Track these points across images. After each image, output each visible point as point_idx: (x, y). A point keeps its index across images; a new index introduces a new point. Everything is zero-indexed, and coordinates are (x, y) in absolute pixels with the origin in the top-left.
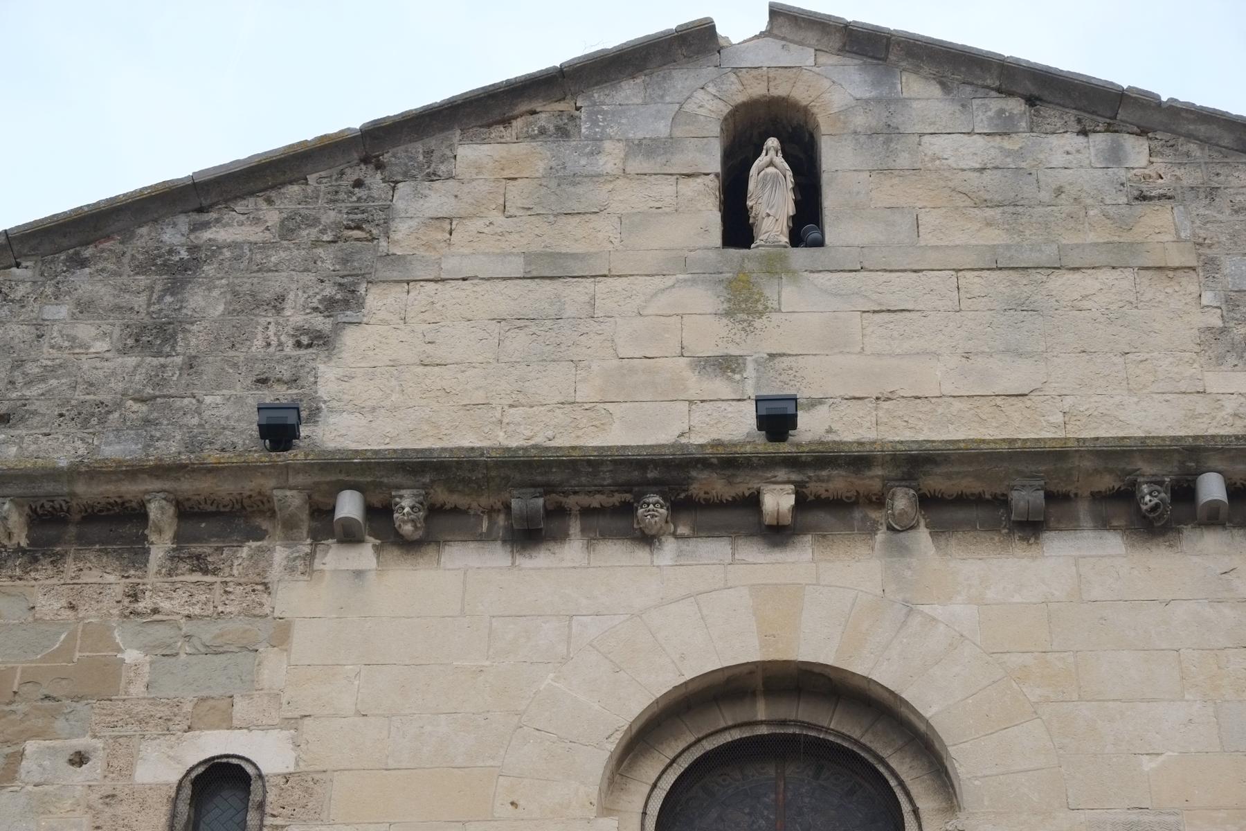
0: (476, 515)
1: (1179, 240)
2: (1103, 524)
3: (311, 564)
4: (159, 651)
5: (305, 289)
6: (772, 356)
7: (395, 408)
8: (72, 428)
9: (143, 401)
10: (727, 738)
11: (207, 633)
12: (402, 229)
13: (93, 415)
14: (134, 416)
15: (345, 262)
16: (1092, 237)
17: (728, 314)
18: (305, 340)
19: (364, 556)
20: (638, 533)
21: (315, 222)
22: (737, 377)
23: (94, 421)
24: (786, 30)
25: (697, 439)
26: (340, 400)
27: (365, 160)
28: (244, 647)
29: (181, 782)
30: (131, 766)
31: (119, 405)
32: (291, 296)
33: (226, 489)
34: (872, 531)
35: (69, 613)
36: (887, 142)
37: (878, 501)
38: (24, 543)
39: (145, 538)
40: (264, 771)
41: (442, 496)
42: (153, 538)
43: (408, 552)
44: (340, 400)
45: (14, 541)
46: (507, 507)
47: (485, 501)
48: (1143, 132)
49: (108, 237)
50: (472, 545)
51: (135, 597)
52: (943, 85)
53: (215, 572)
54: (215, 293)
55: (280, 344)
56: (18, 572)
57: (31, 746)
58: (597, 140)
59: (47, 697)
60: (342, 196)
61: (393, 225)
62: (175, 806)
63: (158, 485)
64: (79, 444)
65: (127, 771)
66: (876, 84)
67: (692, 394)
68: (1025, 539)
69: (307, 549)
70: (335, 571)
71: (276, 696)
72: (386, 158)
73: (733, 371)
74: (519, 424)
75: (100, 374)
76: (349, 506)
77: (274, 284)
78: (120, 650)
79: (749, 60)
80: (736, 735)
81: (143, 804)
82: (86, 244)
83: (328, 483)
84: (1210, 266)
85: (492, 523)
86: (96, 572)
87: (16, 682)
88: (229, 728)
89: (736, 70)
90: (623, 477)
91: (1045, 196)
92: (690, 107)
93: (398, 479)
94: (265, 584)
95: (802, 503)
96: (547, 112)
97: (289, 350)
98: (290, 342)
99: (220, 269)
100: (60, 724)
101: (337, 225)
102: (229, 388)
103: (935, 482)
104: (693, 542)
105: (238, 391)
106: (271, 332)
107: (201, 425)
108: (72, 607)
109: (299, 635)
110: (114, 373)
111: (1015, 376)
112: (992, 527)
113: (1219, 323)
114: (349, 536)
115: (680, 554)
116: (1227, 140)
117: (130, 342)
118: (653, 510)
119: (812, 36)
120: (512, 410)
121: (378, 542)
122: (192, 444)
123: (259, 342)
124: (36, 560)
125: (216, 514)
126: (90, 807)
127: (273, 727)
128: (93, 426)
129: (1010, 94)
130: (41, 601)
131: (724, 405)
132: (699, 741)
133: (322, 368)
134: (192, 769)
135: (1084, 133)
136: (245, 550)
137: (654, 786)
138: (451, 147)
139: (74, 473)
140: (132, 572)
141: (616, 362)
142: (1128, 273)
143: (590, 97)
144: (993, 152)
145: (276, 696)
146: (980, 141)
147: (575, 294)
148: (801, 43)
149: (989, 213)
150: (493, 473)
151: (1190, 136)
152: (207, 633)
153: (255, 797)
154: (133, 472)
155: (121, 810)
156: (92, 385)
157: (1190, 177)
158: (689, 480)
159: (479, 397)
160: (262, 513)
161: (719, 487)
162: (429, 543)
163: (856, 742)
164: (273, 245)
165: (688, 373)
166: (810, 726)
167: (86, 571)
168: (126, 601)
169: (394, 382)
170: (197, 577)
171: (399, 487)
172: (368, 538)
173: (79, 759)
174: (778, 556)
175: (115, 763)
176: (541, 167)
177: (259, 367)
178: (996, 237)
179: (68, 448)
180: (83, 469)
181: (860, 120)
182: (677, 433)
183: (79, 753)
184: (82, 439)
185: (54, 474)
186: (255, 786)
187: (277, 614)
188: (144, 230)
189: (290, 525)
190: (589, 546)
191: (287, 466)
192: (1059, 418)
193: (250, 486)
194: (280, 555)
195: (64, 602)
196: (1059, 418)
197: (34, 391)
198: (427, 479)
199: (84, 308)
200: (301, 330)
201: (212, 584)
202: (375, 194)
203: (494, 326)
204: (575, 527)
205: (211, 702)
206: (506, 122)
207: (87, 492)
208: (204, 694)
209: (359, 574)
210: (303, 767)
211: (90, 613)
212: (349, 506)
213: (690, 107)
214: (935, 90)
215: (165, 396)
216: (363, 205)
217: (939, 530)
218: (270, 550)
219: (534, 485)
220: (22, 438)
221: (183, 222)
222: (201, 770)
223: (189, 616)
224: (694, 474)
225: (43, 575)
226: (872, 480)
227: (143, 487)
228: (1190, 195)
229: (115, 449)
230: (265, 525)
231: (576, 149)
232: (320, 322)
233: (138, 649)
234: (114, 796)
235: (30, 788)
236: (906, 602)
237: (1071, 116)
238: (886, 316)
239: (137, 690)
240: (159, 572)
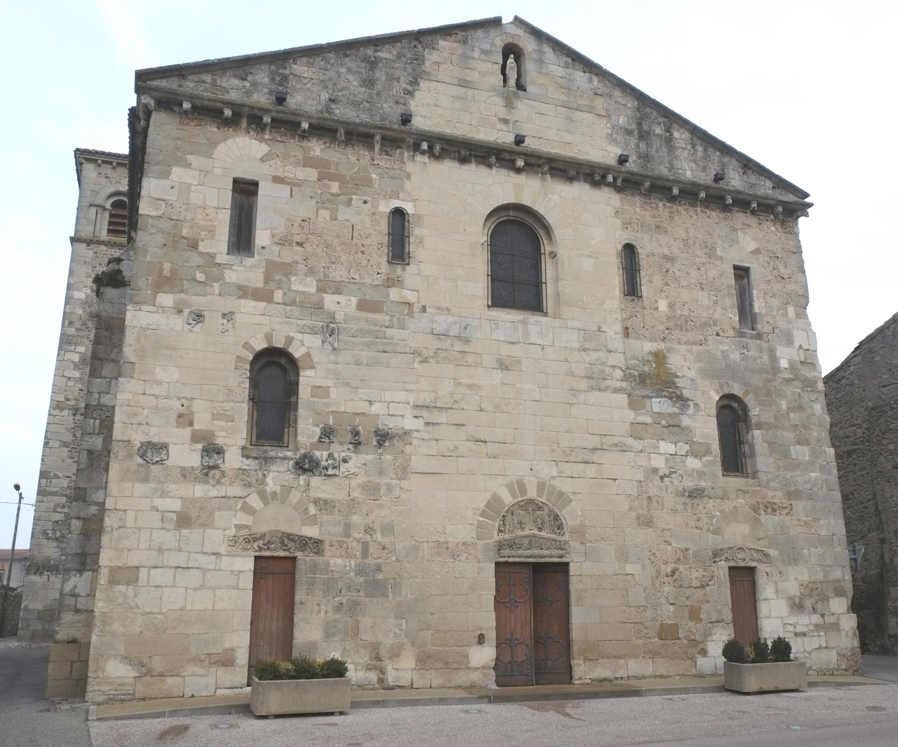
1: (603, 108)
2: (585, 181)
5: (405, 76)
6: (516, 121)
10: (504, 219)
11: (391, 173)
12: (427, 63)
15: (414, 70)
16: (585, 103)
17: (506, 107)
18: (406, 93)
19: (425, 159)
21: (405, 56)
23: (357, 106)
24: (517, 23)
25: (500, 141)
27: (416, 39)
30: (378, 206)
31: (362, 102)
32: (401, 78)
33: (395, 135)
34: (538, 173)
35: (357, 161)
36: (541, 64)
37: (539, 166)
41: (445, 146)
42: (376, 144)
47: (454, 149)
48: (597, 75)
49: (353, 49)
51: (373, 160)
52: (553, 50)
53: (391, 156)
54: (382, 73)
55: (400, 92)
58: (473, 47)
60: (411, 49)
61: (425, 61)
62: (389, 219)
63: (380, 131)
66: (538, 45)
67: (498, 128)
68: (569, 182)
72: (421, 39)
75: (356, 92)
77: (398, 73)
79: (508, 31)
80: (506, 218)
82: (347, 50)
84: (609, 116)
89: (505, 33)
91: (575, 88)
92: (495, 42)
93: (437, 141)
95: (526, 164)
96: (460, 35)
97: (402, 94)
98: (402, 93)
99: (383, 66)
100: (359, 192)
101: (411, 59)
103: (554, 165)
104: (500, 169)
105: (391, 104)
106: (397, 88)
108: (358, 160)
110: (360, 92)
111: (568, 138)
112: (563, 177)
113: (610, 132)
114: (423, 153)
115: (497, 171)
116: (615, 82)
117: (362, 83)
118: (493, 160)
119: (524, 27)
123: (395, 91)
125: (390, 140)
127: (409, 201)
129: (568, 56)
130: (350, 157)
133: (411, 102)
135: (584, 72)
138: (438, 40)
139: (360, 124)
142: (592, 115)
143: (470, 32)
144: (564, 73)
146: (561, 69)
147: (470, 92)
148: (521, 28)
149: (563, 90)
151: (607, 79)
152: (391, 173)
154: (375, 127)
157: (606, 91)
159: (449, 118)
161: (507, 156)
163: (531, 224)
164: (396, 61)
165: (497, 122)
166: (522, 219)
169: (429, 110)
170: (387, 157)
173: (365, 202)
174: (518, 176)
176: (460, 52)
177: (396, 98)
178: (564, 98)
181: (534, 56)
185: (355, 124)
186: (406, 216)
188: (362, 49)
189: (408, 147)
190: (477, 165)
192: (576, 151)
193: (401, 136)
194: (406, 154)
196: (576, 151)
197: (340, 94)
199: (349, 70)
200: (405, 89)
202: (420, 51)
203: (451, 98)
204: (473, 160)
206: (450, 35)
207: (361, 129)
208: (392, 189)
209: (425, 163)
210: (417, 213)
212: (425, 146)
213: (495, 42)
214: (551, 51)
216: (417, 54)
217: (552, 176)
221: (372, 48)
225: (349, 149)
226: (540, 162)
228: (606, 96)
230: (402, 145)
231: (468, 48)
232: (409, 88)
236: (545, 193)
237: (581, 66)
238: (541, 115)
239: (376, 186)
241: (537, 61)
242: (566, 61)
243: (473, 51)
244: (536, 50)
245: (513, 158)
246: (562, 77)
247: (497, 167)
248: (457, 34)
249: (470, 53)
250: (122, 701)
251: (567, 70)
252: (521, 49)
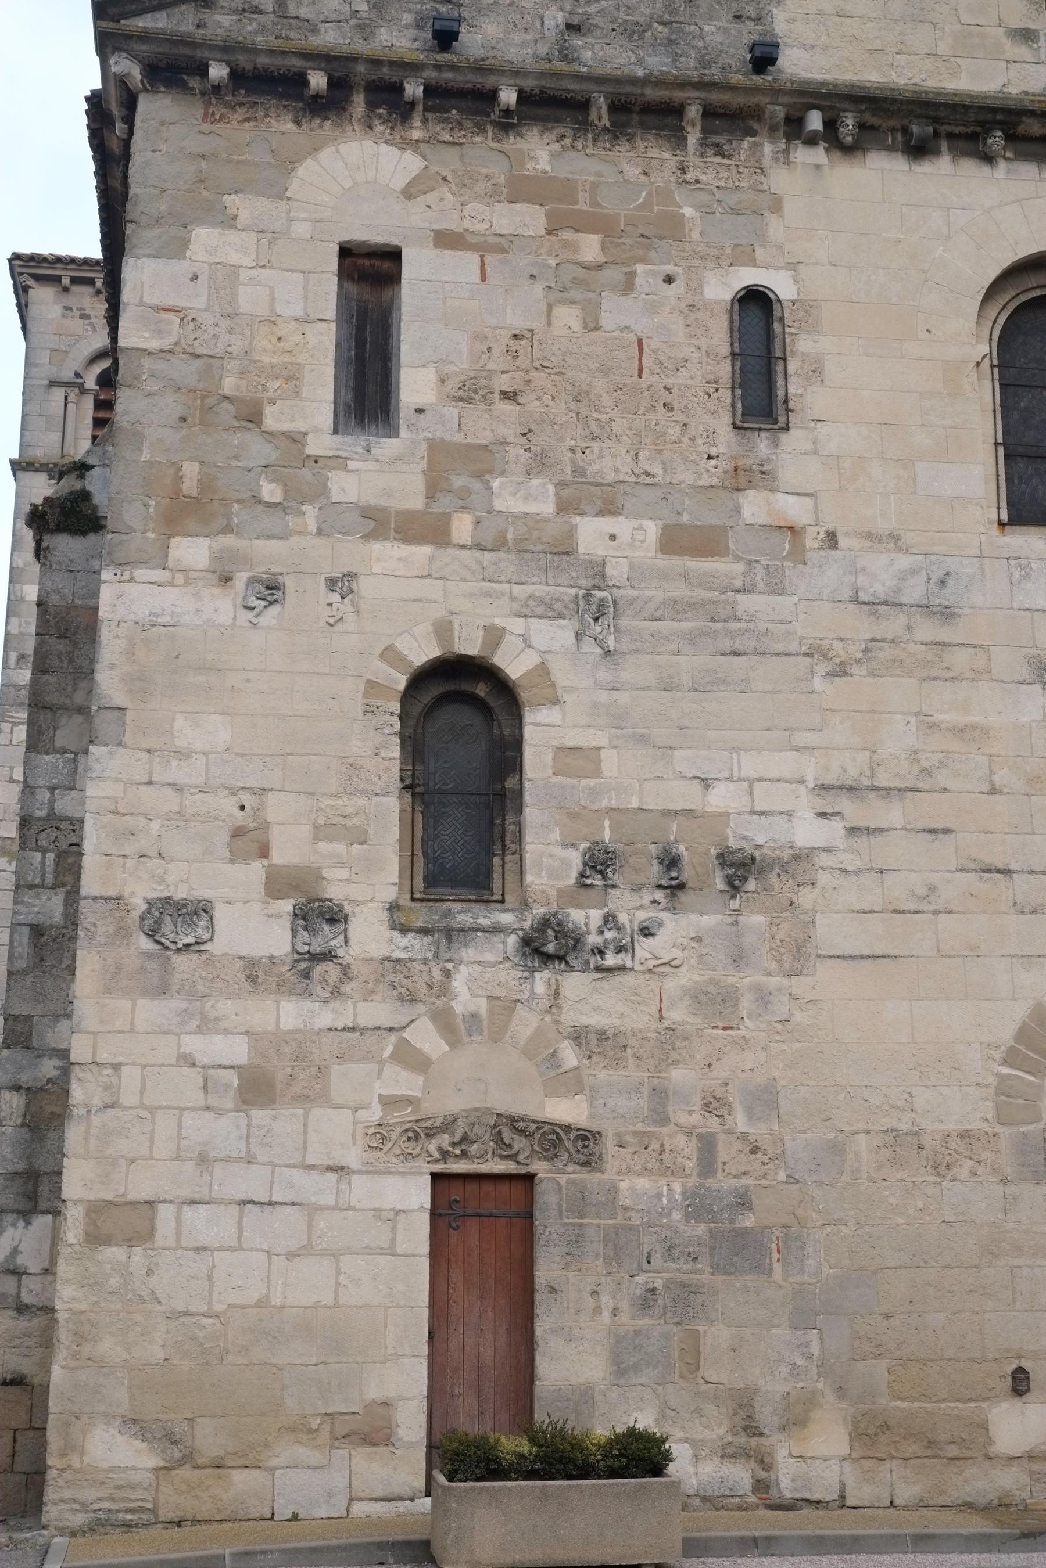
0: (884, 131)
3: (788, 158)
4: (704, 210)
7: (825, 48)
8: (622, 40)
9: (663, 24)
11: (732, 199)
13: (634, 32)
14: (661, 35)
19: (818, 155)
20: (982, 154)
22: (1035, 46)
23: (636, 37)
25: (1014, 90)
26: (789, 37)
28: (755, 212)
29: (732, 300)
33: (738, 100)
35: (643, 178)
38: (608, 124)
39: (682, 129)
40: (781, 297)
41: (870, 119)
42: (689, 129)
43: (846, 154)
44: (789, 37)
45: (602, 123)
46: (905, 130)
50: (884, 153)
51: (683, 170)
53: (729, 157)
56: (608, 145)
57: (640, 268)
59: (642, 235)
62: (731, 316)
64: (630, 53)
65: (699, 290)
69: (784, 146)
70: (803, 163)
71: (780, 248)
73: (1032, 41)
74: (903, 67)
76: (815, 121)
78: (681, 207)
81: (712, 312)
83: (801, 103)
85: (894, 139)
86: (655, 150)
87: (622, 223)
88: (754, 266)
90: (981, 117)
93: (846, 105)
94: (761, 169)
100: (652, 254)
102: (718, 21)
104: (1016, 164)
105: (723, 23)
107: (705, 48)
108: (646, 174)
109: (788, 206)
114: (811, 141)
115: (1009, 172)
118: (996, 141)
120: (898, 56)
121: (826, 145)
122: (704, 63)
124: (616, 138)
126: (681, 312)
127: (781, 268)
128: (636, 41)
130: (626, 168)
131: (1028, 66)
132: (1018, 295)
133: (775, 11)
134: (738, 292)
136: (746, 143)
137: (995, 322)
140: (678, 152)
141: (959, 27)
145: (780, 248)
150: (904, 107)
152: (732, 199)
153: (777, 313)
154: (684, 84)
155: (700, 315)
156: (629, 8)
158: (1020, 122)
159: (877, 45)
160: (752, 117)
162: (858, 149)
165: (1004, 40)
167: (650, 149)
168: (679, 172)
169: (822, 28)
171: (845, 111)
172: (821, 142)
173: (669, 280)
175: (691, 284)
179: (624, 56)
180: (653, 79)
182: (1001, 84)
183: (668, 275)
184: (632, 50)
186: (776, 307)
187: (772, 191)
189: (773, 129)
190: (954, 160)
191: (780, 90)
194: (768, 148)
195: (640, 170)
198: (863, 107)
201: (729, 165)
204: (944, 146)
205: (741, 248)
207: (651, 94)
208: (736, 242)
209: (818, 167)
210: (802, 296)
211: (658, 179)
212: (815, 121)
215: (677, 22)
218: (762, 145)
219: (927, 117)
220: (593, 45)
222: (743, 293)
223: (718, 187)
224: (1024, 119)
225: (623, 149)
227: (687, 95)
229: (658, 63)
230: (756, 126)
233: (691, 207)
234: (694, 306)
235: (644, 296)
239: (695, 235)
240: (695, 154)
247: (1007, 159)
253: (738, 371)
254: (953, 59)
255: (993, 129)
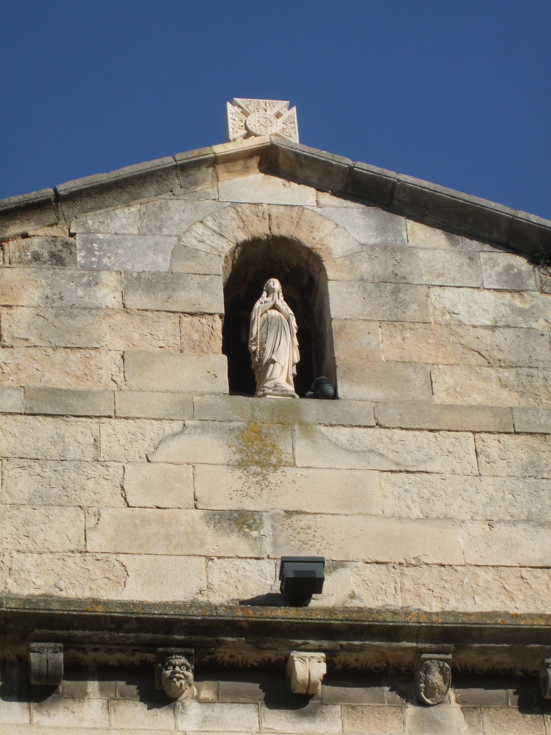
6: (289, 513)
17: (242, 465)
22: (255, 534)
36: (395, 292)
66: (382, 229)
73: (250, 527)
104: (218, 707)
131: (243, 563)
144: (503, 310)
149: (505, 374)
165: (201, 526)
182: (195, 590)
213: (191, 241)
231: (72, 278)
241: (377, 285)
242: (509, 267)
243: (94, 283)
244: (372, 247)
245: (270, 655)
246: (493, 328)
247: (202, 701)
248: (25, 236)
249: (80, 293)
250: (241, 218)
251: (517, 302)
252: (310, 251)
253: (491, 627)
254: (113, 557)
255: (171, 654)
